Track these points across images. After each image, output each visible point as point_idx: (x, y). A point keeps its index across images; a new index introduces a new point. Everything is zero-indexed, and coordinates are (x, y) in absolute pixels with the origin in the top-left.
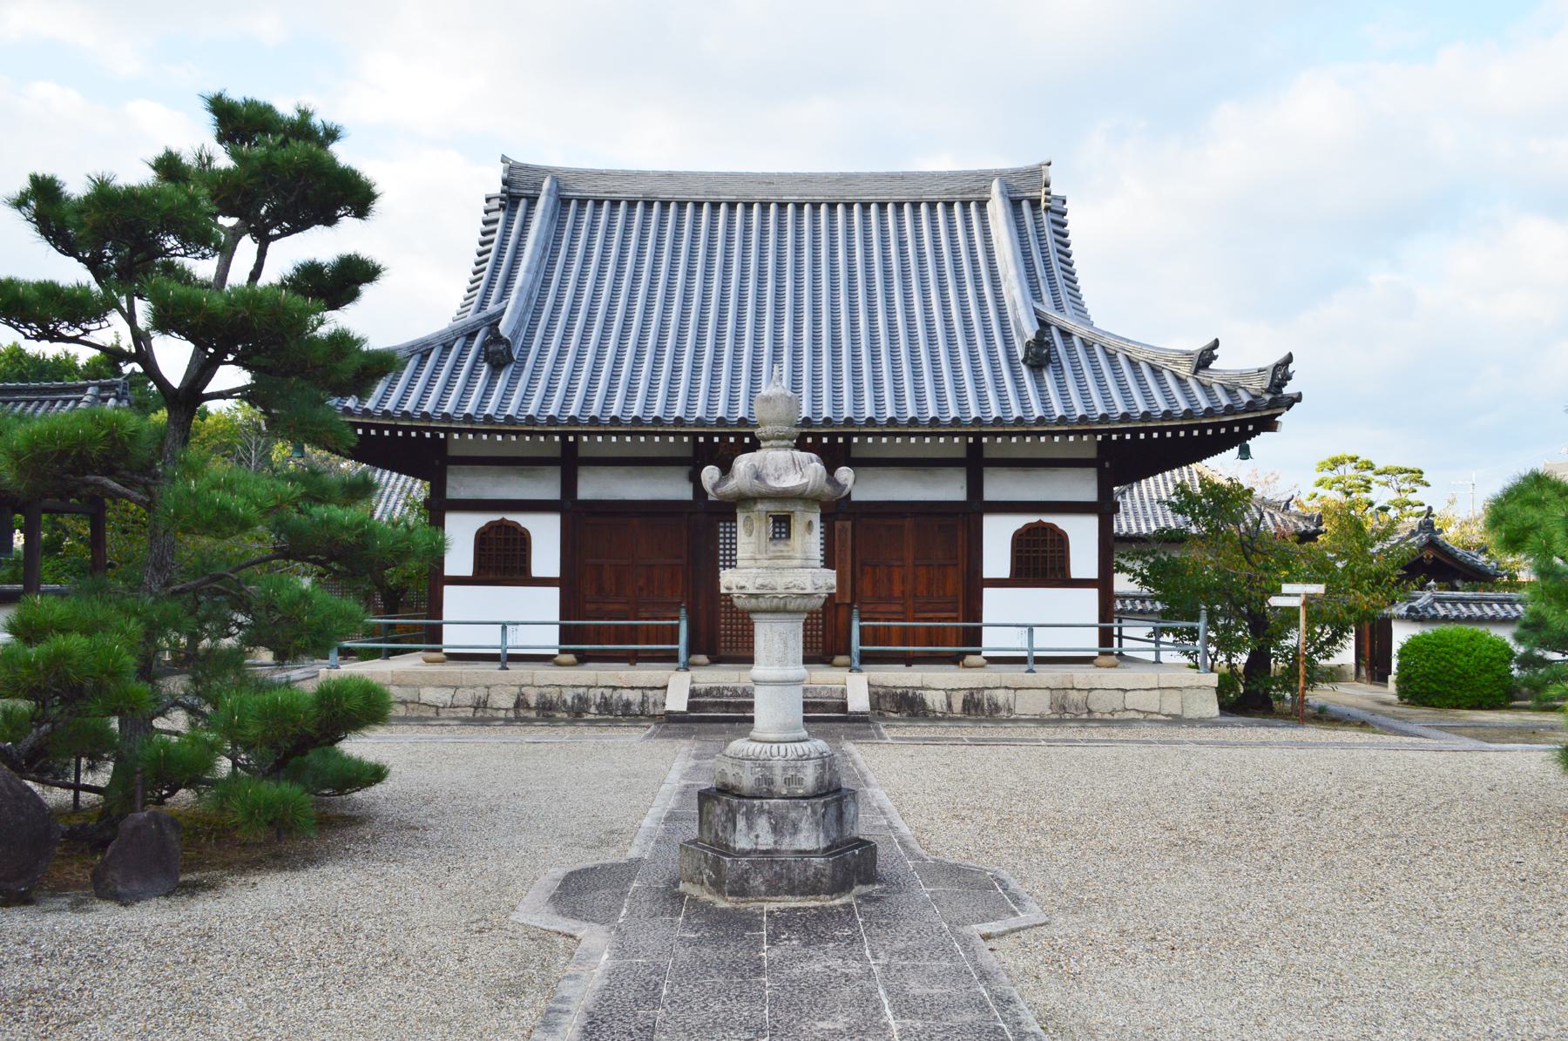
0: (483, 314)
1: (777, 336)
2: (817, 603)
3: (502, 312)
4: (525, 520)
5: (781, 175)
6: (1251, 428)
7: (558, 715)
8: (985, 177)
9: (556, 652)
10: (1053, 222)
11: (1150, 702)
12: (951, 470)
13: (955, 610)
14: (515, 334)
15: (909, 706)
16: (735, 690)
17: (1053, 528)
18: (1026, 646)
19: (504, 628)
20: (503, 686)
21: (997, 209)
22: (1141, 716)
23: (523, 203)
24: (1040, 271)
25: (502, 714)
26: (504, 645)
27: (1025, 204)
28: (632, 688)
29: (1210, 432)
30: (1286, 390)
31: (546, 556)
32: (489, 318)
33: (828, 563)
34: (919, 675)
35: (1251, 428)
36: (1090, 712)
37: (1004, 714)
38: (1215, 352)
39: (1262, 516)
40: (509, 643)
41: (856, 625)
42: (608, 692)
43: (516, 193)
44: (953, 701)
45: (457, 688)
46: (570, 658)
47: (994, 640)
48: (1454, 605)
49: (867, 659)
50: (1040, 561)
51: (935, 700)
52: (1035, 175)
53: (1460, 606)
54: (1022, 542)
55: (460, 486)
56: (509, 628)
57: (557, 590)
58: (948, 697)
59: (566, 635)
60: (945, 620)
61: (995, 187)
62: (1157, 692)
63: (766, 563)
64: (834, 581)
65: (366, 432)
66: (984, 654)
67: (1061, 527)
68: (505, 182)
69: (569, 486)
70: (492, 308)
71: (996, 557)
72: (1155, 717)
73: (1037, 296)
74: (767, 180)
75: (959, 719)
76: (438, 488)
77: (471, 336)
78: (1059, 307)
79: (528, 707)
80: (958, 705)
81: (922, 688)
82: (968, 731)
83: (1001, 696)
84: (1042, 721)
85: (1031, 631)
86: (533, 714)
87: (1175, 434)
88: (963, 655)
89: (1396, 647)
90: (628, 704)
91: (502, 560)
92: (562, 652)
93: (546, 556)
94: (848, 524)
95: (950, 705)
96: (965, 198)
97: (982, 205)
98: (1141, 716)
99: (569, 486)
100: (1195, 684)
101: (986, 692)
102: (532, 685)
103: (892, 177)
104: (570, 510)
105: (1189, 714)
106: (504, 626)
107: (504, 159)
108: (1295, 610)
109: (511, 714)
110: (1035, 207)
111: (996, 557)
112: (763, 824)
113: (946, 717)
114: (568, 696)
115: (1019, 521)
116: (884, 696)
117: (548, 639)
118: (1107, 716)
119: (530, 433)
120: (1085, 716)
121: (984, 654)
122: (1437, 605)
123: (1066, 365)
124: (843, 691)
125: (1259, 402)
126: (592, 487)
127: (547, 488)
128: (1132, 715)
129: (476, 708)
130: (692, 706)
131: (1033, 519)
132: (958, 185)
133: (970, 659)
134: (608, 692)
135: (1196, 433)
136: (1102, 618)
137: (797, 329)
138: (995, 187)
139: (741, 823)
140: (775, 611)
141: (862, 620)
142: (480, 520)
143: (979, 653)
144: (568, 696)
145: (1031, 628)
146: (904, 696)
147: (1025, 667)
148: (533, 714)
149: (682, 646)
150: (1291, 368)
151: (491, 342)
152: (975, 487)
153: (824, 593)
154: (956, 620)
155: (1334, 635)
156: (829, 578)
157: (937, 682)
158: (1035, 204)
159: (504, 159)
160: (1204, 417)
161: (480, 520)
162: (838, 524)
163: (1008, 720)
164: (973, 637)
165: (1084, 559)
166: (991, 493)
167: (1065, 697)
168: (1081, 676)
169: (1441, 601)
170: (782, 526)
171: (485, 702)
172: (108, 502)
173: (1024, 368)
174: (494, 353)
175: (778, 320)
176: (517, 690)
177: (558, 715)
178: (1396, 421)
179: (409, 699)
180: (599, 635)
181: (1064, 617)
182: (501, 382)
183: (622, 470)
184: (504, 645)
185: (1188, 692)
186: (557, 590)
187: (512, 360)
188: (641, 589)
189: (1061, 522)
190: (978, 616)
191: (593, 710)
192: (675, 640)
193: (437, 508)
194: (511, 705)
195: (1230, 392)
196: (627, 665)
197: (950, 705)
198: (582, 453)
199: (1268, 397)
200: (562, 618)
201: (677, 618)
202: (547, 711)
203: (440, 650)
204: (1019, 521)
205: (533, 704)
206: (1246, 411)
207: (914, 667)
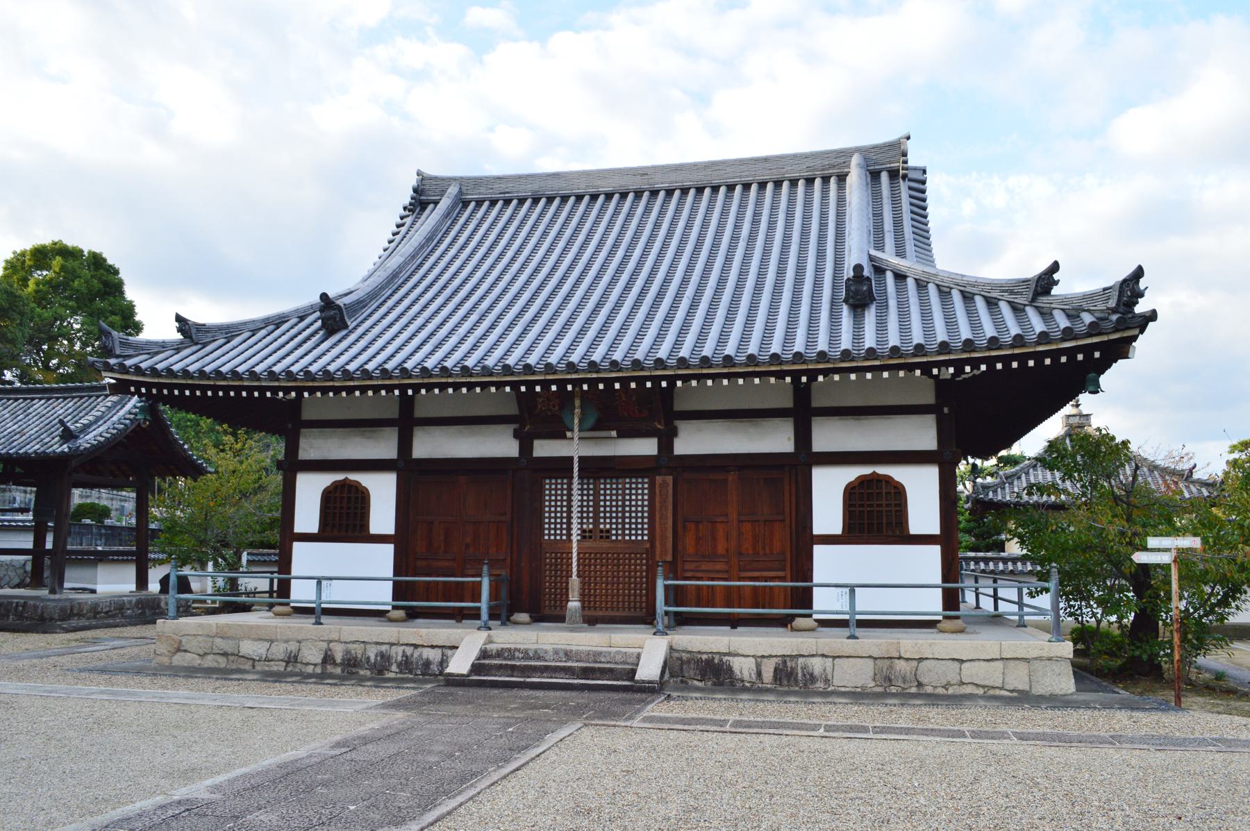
5: (654, 168)
7: (362, 672)
8: (846, 154)
9: (389, 608)
10: (910, 188)
11: (992, 675)
12: (777, 421)
13: (783, 570)
15: (715, 674)
16: (526, 652)
17: (888, 480)
18: (847, 608)
19: (319, 583)
20: (312, 640)
21: (855, 178)
22: (981, 692)
24: (888, 225)
25: (310, 669)
26: (853, 610)
28: (432, 647)
29: (1048, 361)
31: (382, 517)
36: (920, 685)
37: (820, 685)
40: (858, 609)
41: (660, 584)
42: (409, 650)
43: (420, 201)
44: (763, 668)
45: (272, 641)
46: (400, 614)
47: (826, 602)
50: (876, 515)
51: (743, 667)
52: (897, 149)
55: (311, 448)
56: (324, 583)
57: (392, 546)
58: (758, 666)
59: (400, 591)
61: (855, 160)
62: (1000, 664)
66: (815, 616)
67: (896, 479)
68: (415, 190)
69: (405, 445)
71: (827, 514)
72: (998, 692)
73: (880, 246)
74: (643, 172)
75: (767, 691)
76: (292, 448)
78: (900, 253)
79: (334, 664)
80: (768, 675)
82: (771, 710)
83: (817, 665)
84: (858, 696)
85: (852, 592)
86: (338, 670)
87: (1007, 365)
88: (793, 617)
90: (427, 664)
91: (344, 518)
92: (394, 608)
93: (382, 517)
94: (670, 479)
95: (759, 674)
96: (825, 172)
97: (842, 178)
98: (981, 692)
99: (405, 445)
101: (801, 660)
102: (339, 641)
104: (407, 469)
105: (1038, 690)
106: (319, 581)
108: (1166, 568)
109: (318, 670)
110: (891, 171)
111: (827, 514)
113: (755, 689)
114: (372, 653)
116: (689, 661)
117: (382, 594)
118: (941, 691)
120: (914, 690)
123: (892, 303)
124: (638, 656)
125: (1104, 325)
126: (428, 445)
127: (385, 447)
128: (969, 690)
129: (288, 662)
130: (476, 668)
131: (866, 470)
132: (818, 162)
133: (800, 622)
134: (409, 650)
136: (947, 577)
138: (855, 160)
141: (666, 578)
142: (326, 480)
143: (810, 616)
144: (372, 653)
145: (852, 588)
146: (709, 663)
147: (845, 632)
148: (338, 670)
149: (484, 604)
150: (1142, 284)
152: (803, 436)
154: (783, 579)
155: (1226, 596)
157: (750, 648)
158: (894, 174)
160: (1038, 343)
161: (326, 480)
162: (659, 479)
163: (825, 694)
164: (804, 599)
165: (924, 514)
167: (891, 667)
168: (910, 642)
171: (296, 657)
173: (845, 308)
176: (325, 645)
177: (362, 672)
179: (230, 651)
180: (429, 592)
181: (905, 575)
184: (853, 610)
185: (1037, 664)
186: (392, 546)
188: (467, 546)
189: (897, 473)
190: (808, 576)
191: (394, 668)
192: (476, 597)
193: (292, 466)
194: (319, 660)
195: (1072, 315)
196: (453, 622)
197: (759, 674)
199: (1114, 317)
200: (395, 575)
201: (480, 576)
203: (288, 604)
205: (339, 660)
206: (1089, 335)
207: (740, 629)
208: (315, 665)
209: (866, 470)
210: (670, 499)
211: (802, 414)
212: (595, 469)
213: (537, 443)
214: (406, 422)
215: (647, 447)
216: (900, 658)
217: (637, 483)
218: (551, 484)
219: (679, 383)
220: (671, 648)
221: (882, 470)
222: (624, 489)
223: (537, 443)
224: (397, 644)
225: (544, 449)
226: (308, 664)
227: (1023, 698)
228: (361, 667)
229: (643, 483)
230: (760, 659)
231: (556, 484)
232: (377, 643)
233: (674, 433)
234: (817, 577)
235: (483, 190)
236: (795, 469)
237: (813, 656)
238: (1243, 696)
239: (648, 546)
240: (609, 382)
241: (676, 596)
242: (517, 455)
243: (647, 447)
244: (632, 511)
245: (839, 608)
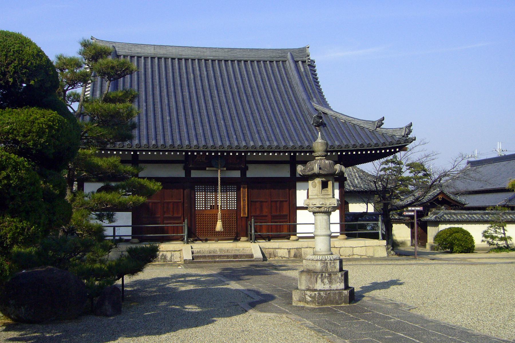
6: (397, 150)
9: (130, 238)
27: (300, 62)
30: (410, 136)
34: (278, 244)
35: (397, 150)
38: (383, 122)
48: (451, 215)
52: (303, 51)
53: (453, 216)
56: (116, 228)
57: (297, 206)
60: (282, 222)
63: (322, 197)
65: (342, 153)
66: (298, 235)
89: (465, 227)
97: (284, 62)
98: (359, 257)
100: (378, 244)
103: (251, 50)
105: (377, 256)
112: (326, 281)
121: (298, 235)
122: (445, 215)
128: (356, 257)
133: (293, 238)
135: (354, 153)
139: (319, 281)
150: (412, 128)
152: (293, 171)
158: (304, 62)
169: (446, 214)
178: (442, 147)
183: (157, 165)
198: (297, 159)
211: (293, 162)
213: (192, 172)
215: (237, 174)
217: (232, 188)
218: (197, 188)
219: (297, 154)
223: (192, 172)
225: (195, 174)
227: (371, 259)
229: (234, 188)
231: (200, 188)
233: (247, 168)
235: (127, 51)
237: (277, 249)
238: (513, 250)
242: (184, 176)
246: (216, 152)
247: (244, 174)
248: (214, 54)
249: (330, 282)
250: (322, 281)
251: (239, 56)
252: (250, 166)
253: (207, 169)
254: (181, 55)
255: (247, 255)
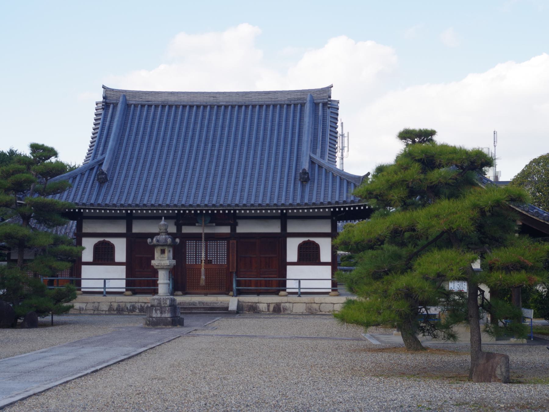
0: (96, 160)
1: (209, 169)
2: (172, 267)
3: (104, 159)
4: (112, 240)
7: (125, 313)
9: (124, 290)
14: (108, 169)
15: (254, 309)
17: (314, 243)
20: (105, 302)
23: (111, 106)
31: (120, 255)
32: (98, 162)
33: (174, 259)
34: (249, 298)
39: (50, 267)
41: (234, 280)
45: (87, 303)
47: (291, 285)
49: (240, 293)
51: (263, 307)
54: (302, 248)
55: (87, 228)
56: (107, 281)
57: (125, 267)
59: (128, 283)
64: (175, 263)
66: (288, 290)
67: (317, 242)
68: (104, 98)
69: (129, 227)
70: (99, 157)
71: (292, 255)
73: (314, 152)
77: (92, 169)
80: (271, 308)
81: (258, 303)
86: (115, 313)
93: (120, 255)
94: (235, 241)
99: (129, 227)
101: (282, 304)
102: (115, 302)
107: (104, 87)
109: (107, 313)
111: (292, 255)
112: (158, 312)
114: (128, 306)
115: (301, 240)
119: (114, 210)
121: (288, 290)
124: (228, 304)
131: (306, 239)
133: (282, 293)
134: (143, 305)
137: (217, 166)
139: (154, 311)
140: (162, 269)
143: (285, 290)
144: (128, 306)
145: (299, 280)
151: (100, 174)
152: (284, 227)
153: (172, 265)
156: (174, 262)
157: (265, 301)
159: (104, 87)
161: (96, 240)
162: (231, 241)
163: (289, 314)
164: (283, 284)
166: (290, 230)
168: (317, 299)
170: (163, 252)
172: (493, 330)
174: (101, 178)
175: (210, 162)
180: (141, 283)
182: (103, 190)
186: (125, 267)
187: (107, 180)
189: (317, 240)
190: (285, 275)
193: (80, 235)
194: (107, 309)
200: (127, 277)
202: (120, 311)
204: (301, 240)
208: (106, 311)
209: (306, 239)
210: (235, 249)
211: (284, 218)
212: (210, 237)
213: (183, 227)
214: (129, 218)
215: (226, 230)
216: (314, 303)
220: (239, 301)
221: (312, 239)
222: (217, 245)
223: (183, 227)
224: (139, 302)
225: (186, 230)
226: (102, 311)
228: (125, 311)
230: (269, 305)
232: (130, 302)
234: (288, 276)
235: (137, 99)
236: (278, 243)
239: (227, 266)
240: (213, 211)
241: (239, 283)
243: (226, 230)
244: (220, 255)
245: (295, 287)
246: (201, 211)
247: (233, 229)
248: (227, 99)
249: (161, 313)
250: (156, 312)
251: (254, 100)
252: (239, 221)
253: (197, 224)
254: (193, 102)
255: (222, 308)
